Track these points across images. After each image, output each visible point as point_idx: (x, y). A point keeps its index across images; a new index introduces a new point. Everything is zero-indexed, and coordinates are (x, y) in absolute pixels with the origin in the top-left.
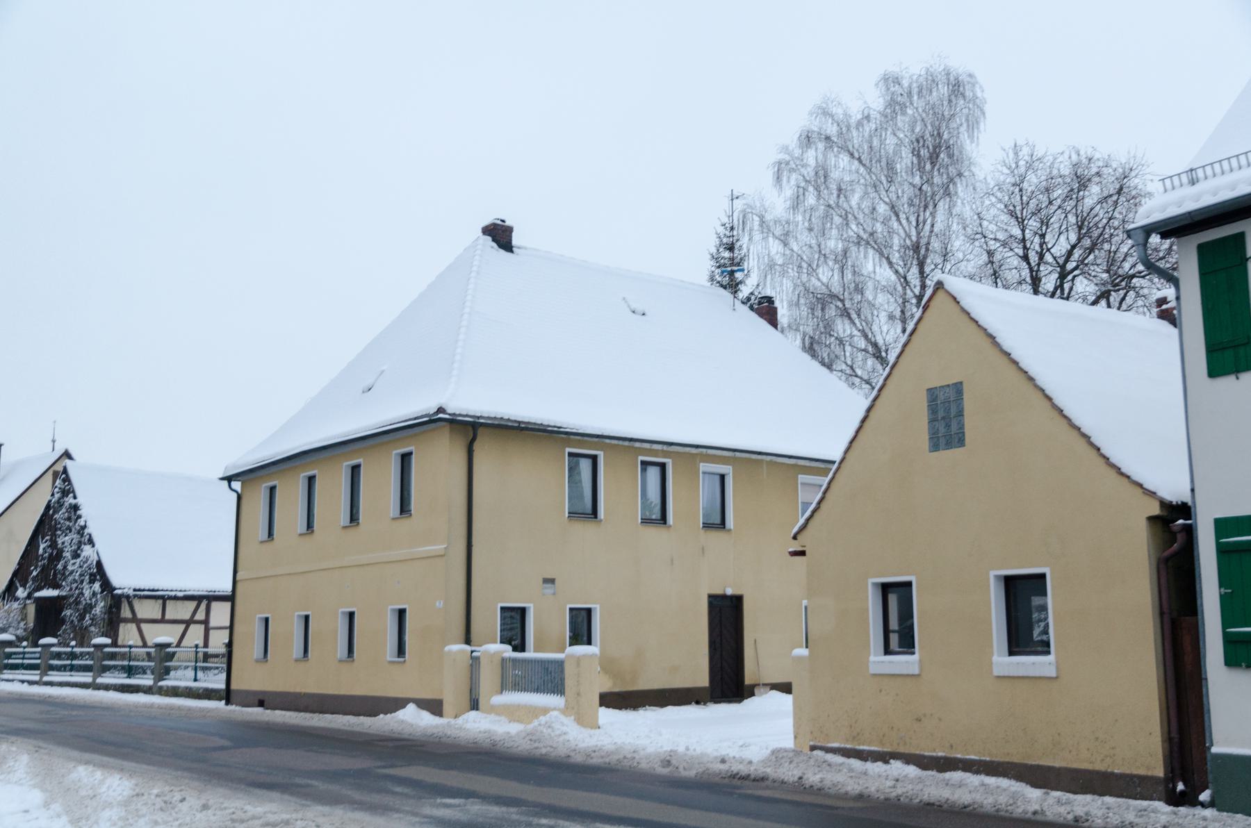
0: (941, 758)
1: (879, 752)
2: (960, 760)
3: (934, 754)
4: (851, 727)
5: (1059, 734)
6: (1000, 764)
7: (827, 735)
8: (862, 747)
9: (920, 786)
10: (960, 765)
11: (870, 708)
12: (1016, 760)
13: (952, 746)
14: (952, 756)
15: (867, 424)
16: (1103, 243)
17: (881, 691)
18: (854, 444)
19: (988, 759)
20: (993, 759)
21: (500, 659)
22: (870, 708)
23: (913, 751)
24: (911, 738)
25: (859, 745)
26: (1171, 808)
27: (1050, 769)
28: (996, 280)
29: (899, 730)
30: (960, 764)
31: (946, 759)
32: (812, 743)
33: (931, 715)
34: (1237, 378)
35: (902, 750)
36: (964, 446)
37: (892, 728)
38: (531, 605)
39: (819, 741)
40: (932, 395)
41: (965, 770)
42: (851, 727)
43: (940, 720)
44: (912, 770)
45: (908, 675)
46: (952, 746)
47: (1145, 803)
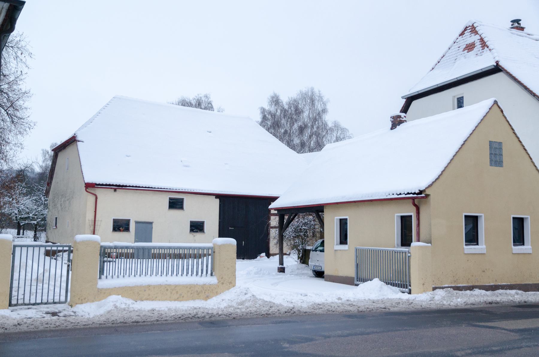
0: (493, 285)
2: (500, 286)
3: (490, 284)
5: (531, 273)
6: (514, 285)
7: (442, 282)
8: (459, 285)
10: (500, 287)
11: (463, 268)
12: (518, 283)
13: (496, 281)
17: (468, 261)
18: (458, 153)
19: (509, 284)
20: (511, 284)
21: (99, 246)
22: (463, 268)
23: (481, 284)
24: (480, 279)
26: (525, 292)
27: (529, 284)
29: (475, 276)
30: (500, 287)
32: (434, 286)
35: (477, 284)
36: (491, 165)
37: (473, 276)
38: (483, 215)
39: (437, 285)
40: (109, 102)
41: (502, 289)
42: (454, 276)
43: (492, 271)
44: (483, 292)
46: (496, 281)
47: (534, 292)
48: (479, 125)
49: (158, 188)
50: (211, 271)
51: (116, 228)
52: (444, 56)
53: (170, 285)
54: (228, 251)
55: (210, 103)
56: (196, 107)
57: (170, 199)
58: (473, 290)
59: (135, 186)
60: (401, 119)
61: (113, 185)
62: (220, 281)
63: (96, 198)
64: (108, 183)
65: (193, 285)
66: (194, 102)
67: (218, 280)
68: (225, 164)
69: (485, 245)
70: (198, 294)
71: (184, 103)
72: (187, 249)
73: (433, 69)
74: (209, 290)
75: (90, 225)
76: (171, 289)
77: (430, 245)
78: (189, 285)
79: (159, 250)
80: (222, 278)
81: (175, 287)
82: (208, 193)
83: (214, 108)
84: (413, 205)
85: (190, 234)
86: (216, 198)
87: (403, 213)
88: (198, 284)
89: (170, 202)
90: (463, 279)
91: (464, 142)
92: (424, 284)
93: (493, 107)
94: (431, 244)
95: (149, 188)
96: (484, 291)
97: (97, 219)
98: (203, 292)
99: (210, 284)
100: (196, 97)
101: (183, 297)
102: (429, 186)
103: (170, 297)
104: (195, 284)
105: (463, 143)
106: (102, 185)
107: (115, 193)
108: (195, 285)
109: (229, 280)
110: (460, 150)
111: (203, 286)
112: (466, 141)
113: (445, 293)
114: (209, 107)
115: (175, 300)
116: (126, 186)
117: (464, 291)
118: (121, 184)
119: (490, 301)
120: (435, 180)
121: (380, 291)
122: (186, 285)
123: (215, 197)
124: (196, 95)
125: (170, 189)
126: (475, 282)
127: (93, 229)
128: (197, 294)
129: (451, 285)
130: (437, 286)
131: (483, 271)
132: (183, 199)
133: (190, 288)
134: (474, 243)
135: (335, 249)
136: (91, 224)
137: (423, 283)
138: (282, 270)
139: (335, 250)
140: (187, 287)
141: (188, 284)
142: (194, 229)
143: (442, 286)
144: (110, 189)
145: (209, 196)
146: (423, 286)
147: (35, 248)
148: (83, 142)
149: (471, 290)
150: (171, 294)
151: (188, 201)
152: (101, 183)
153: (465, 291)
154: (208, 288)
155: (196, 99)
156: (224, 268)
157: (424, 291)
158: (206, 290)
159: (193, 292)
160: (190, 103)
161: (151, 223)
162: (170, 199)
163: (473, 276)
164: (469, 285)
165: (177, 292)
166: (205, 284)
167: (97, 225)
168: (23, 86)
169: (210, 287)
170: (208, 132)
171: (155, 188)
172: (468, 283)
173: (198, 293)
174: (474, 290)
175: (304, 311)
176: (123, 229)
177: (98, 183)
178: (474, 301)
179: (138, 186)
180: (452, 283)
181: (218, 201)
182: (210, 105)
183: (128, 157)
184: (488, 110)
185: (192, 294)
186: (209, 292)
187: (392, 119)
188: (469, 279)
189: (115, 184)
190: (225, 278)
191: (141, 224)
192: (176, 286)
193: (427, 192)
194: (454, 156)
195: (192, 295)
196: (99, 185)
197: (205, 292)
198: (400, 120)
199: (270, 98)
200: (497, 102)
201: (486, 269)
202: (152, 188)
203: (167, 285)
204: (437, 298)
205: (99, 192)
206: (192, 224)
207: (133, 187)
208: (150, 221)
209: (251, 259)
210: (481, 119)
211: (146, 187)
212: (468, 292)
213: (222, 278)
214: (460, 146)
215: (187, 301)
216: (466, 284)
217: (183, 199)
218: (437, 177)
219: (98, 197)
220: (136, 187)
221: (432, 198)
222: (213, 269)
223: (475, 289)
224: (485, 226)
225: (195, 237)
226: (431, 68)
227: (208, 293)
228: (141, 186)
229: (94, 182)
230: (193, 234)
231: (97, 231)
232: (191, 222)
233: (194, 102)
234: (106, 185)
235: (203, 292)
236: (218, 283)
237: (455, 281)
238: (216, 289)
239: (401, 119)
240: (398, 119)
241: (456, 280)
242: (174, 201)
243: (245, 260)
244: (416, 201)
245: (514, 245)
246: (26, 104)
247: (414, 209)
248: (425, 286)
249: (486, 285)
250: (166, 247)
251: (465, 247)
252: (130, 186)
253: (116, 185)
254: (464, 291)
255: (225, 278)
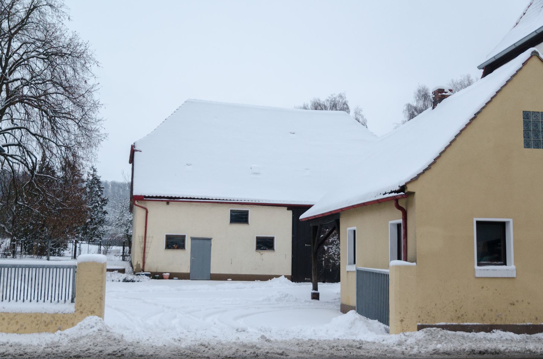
0: (530, 326)
1: (481, 325)
3: (525, 324)
4: (456, 311)
7: (434, 317)
8: (466, 324)
9: (311, 348)
14: (539, 324)
15: (474, 122)
16: (75, 118)
17: (483, 288)
23: (507, 323)
25: (463, 322)
28: (49, 149)
31: (534, 326)
32: (419, 324)
33: (523, 301)
34: (96, 169)
35: (499, 323)
37: (491, 310)
39: (426, 322)
42: (456, 311)
44: (510, 335)
45: (505, 278)
48: (504, 89)
49: (216, 199)
50: (72, 296)
51: (170, 245)
52: (531, 4)
53: (8, 313)
54: (90, 271)
55: (345, 104)
56: (332, 109)
57: (231, 211)
58: (492, 332)
59: (189, 197)
60: (444, 94)
61: (164, 197)
62: (78, 310)
63: (147, 212)
64: (158, 196)
65: (40, 313)
66: (328, 105)
67: (75, 307)
68: (306, 169)
69: (514, 265)
70: (46, 326)
71: (318, 106)
72: (60, 268)
73: (517, 24)
74: (61, 321)
75: (140, 242)
76: (9, 319)
77: (414, 264)
78: (35, 313)
79: (8, 269)
80: (81, 306)
81: (15, 316)
82: (282, 204)
83: (350, 108)
84: (397, 209)
85: (257, 251)
86: (288, 209)
87: (396, 220)
88: (47, 312)
89: (231, 215)
90: (473, 314)
91: (475, 115)
92: (402, 321)
93: (529, 62)
94: (416, 263)
95: (205, 199)
96: (512, 334)
97: (147, 235)
98: (54, 322)
99: (64, 312)
100: (330, 98)
101: (25, 328)
102: (411, 179)
103: (7, 329)
104: (43, 313)
105: (473, 116)
106: (152, 197)
107: (168, 206)
108: (42, 314)
109: (90, 309)
110: (469, 127)
111: (54, 316)
112: (478, 113)
113: (424, 335)
114: (345, 108)
115: (14, 332)
116: (179, 198)
117: (475, 333)
118: (174, 196)
119: (482, 349)
120: (422, 171)
121: (350, 328)
122: (29, 313)
123: (287, 208)
124: (330, 96)
125: (230, 200)
126: (496, 320)
127: (143, 246)
128: (45, 326)
129: (450, 322)
130: (427, 324)
131: (511, 304)
132: (247, 212)
133: (35, 318)
134: (499, 263)
135: (348, 270)
136: (141, 241)
137: (401, 319)
138: (315, 296)
139: (348, 272)
140: (31, 316)
141: (33, 312)
142: (262, 247)
143: (434, 324)
144: (161, 202)
145: (265, 207)
146: (401, 324)
147: (34, 268)
148: (141, 151)
149: (487, 331)
150: (433, 317)
151: (253, 214)
152: (151, 195)
153: (476, 332)
154: (61, 318)
155: (330, 100)
156: (85, 292)
157: (403, 330)
158: (58, 321)
159: (39, 322)
160: (324, 105)
161: (210, 239)
162: (231, 211)
163: (491, 310)
164: (486, 324)
165: (17, 322)
166: (56, 312)
167: (148, 242)
168: (96, 96)
169: (63, 317)
170: (291, 133)
171: (212, 199)
172: (484, 321)
173: (46, 324)
174: (493, 332)
175: (140, 354)
176: (177, 246)
177: (147, 195)
178: (443, 350)
179: (192, 197)
180: (453, 320)
181: (290, 213)
182: (345, 106)
183: (189, 165)
184: (521, 66)
185: (38, 325)
186: (62, 323)
187: (434, 95)
188: (484, 315)
189: (166, 196)
190: (85, 306)
191: (197, 241)
192: (16, 314)
193: (410, 189)
194: (456, 136)
195: (37, 327)
196: (149, 197)
197: (56, 324)
198: (442, 95)
199: (416, 91)
200: (537, 53)
201: (517, 301)
202: (209, 199)
203: (3, 312)
204: (411, 341)
205: (151, 206)
206: (259, 240)
207: (187, 198)
208: (209, 237)
209: (334, 282)
210: (506, 80)
211: (201, 199)
212: (482, 334)
213: (81, 306)
214: (468, 121)
215: (30, 333)
216: (480, 323)
217: (247, 212)
218: (427, 166)
219: (148, 211)
220: (190, 198)
221: (417, 198)
222: (74, 294)
223: (494, 331)
224: (514, 236)
225: (263, 255)
226: (514, 24)
227: (61, 324)
228: (196, 197)
229: (143, 195)
230: (260, 252)
231: (148, 249)
232: (258, 238)
233: (328, 105)
234: (156, 197)
235: (54, 322)
236: (75, 311)
237: (459, 317)
238: (71, 319)
239: (444, 94)
240: (440, 94)
241: (460, 316)
242: (236, 214)
243: (326, 283)
244: (401, 203)
245: (479, 265)
246: (99, 117)
247: (400, 213)
248: (404, 323)
249: (518, 324)
250: (9, 265)
251: (476, 267)
252: (183, 198)
253: (168, 198)
254: (475, 332)
255: (85, 306)
